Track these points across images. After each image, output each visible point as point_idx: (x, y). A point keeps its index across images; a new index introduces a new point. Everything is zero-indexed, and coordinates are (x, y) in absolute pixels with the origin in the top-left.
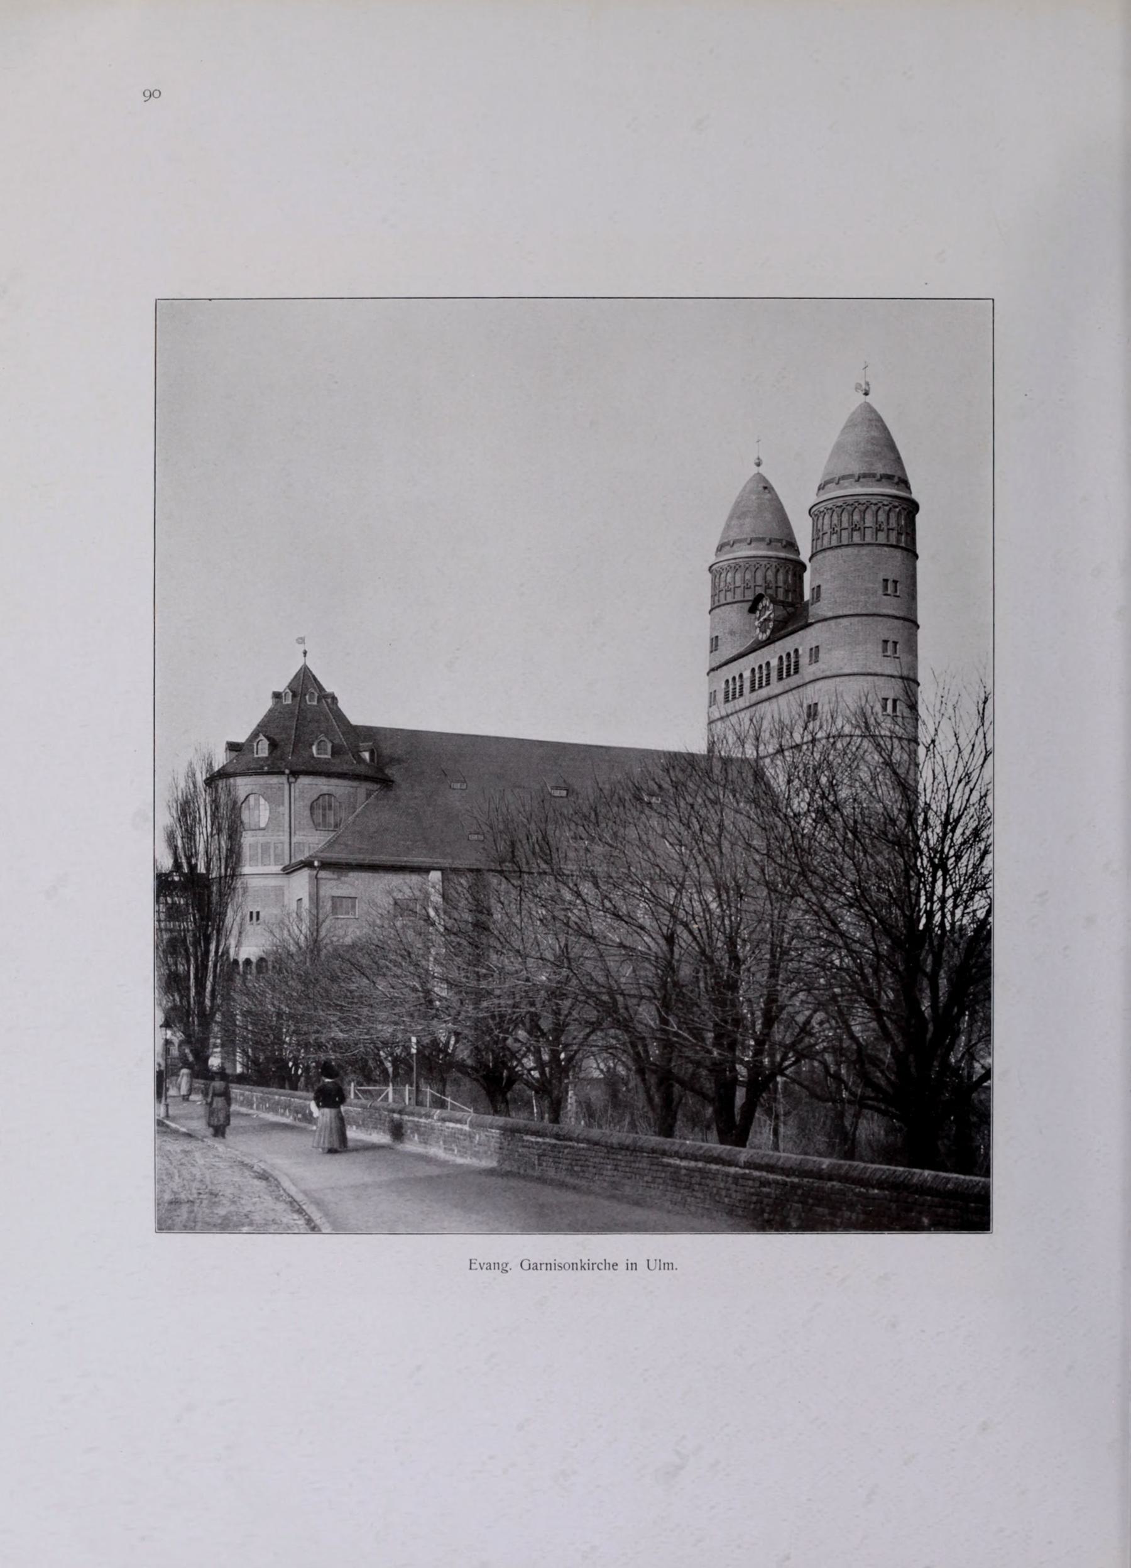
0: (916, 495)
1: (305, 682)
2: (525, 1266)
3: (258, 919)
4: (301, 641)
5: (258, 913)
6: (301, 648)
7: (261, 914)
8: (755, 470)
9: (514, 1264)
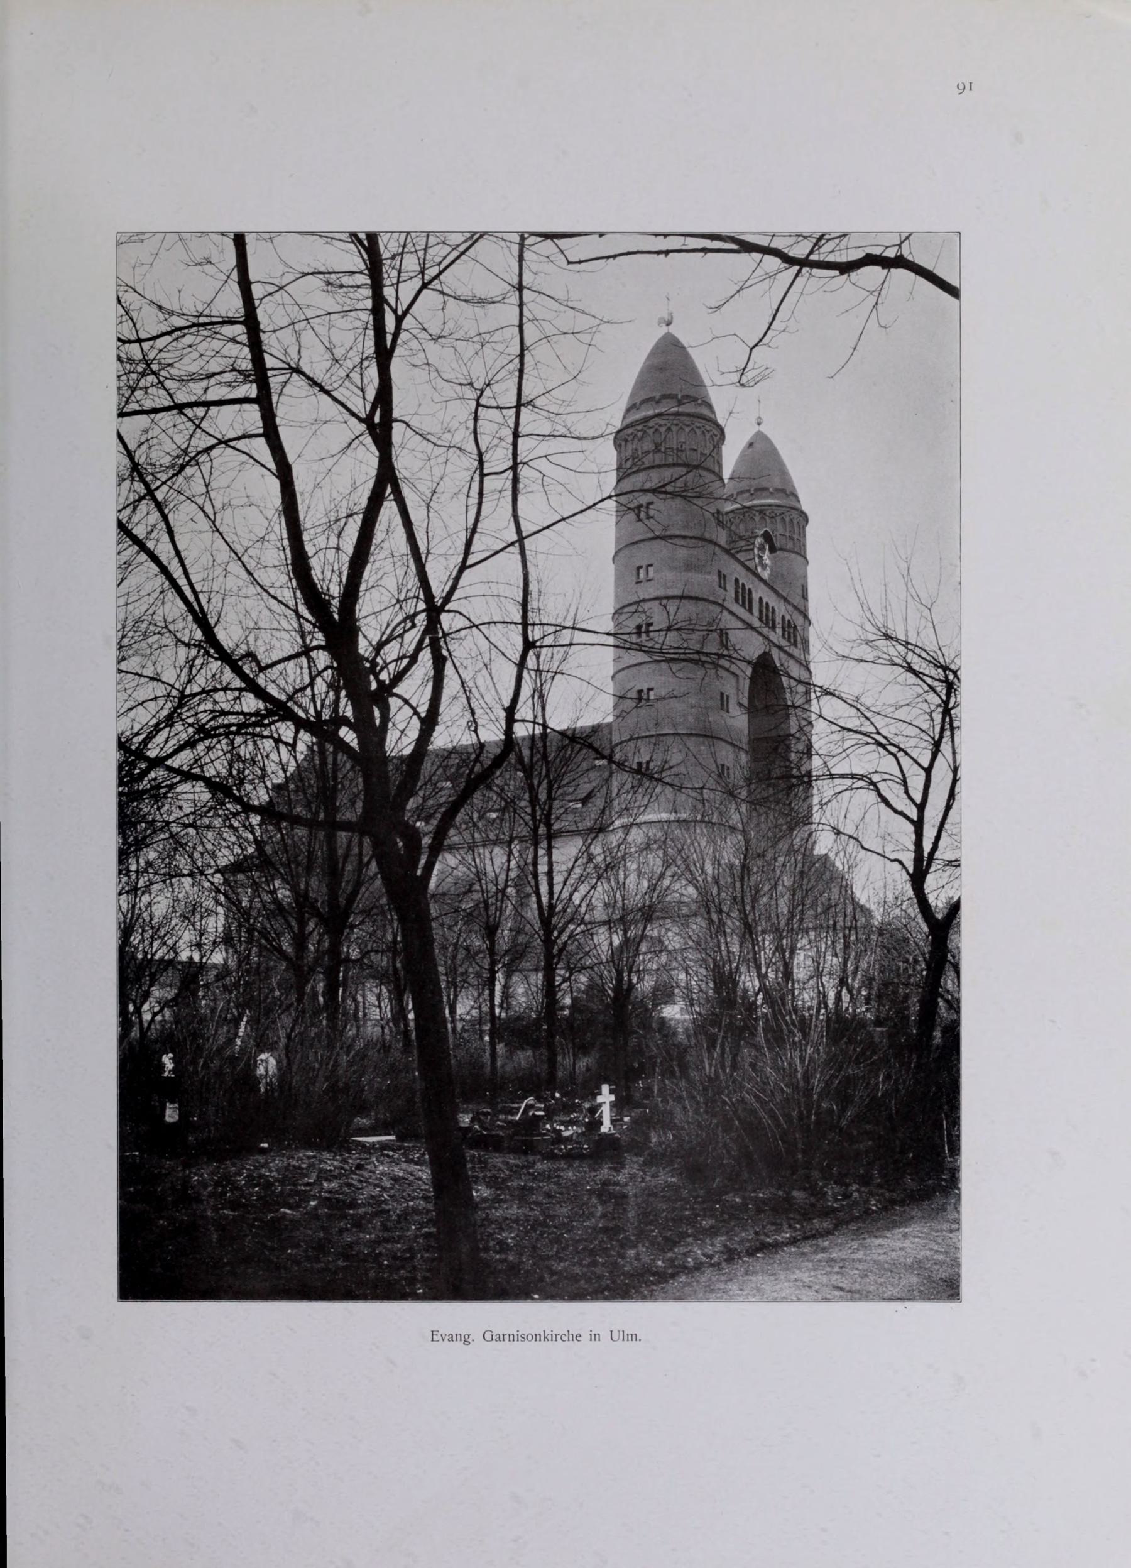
2: (488, 1337)
9: (477, 1336)
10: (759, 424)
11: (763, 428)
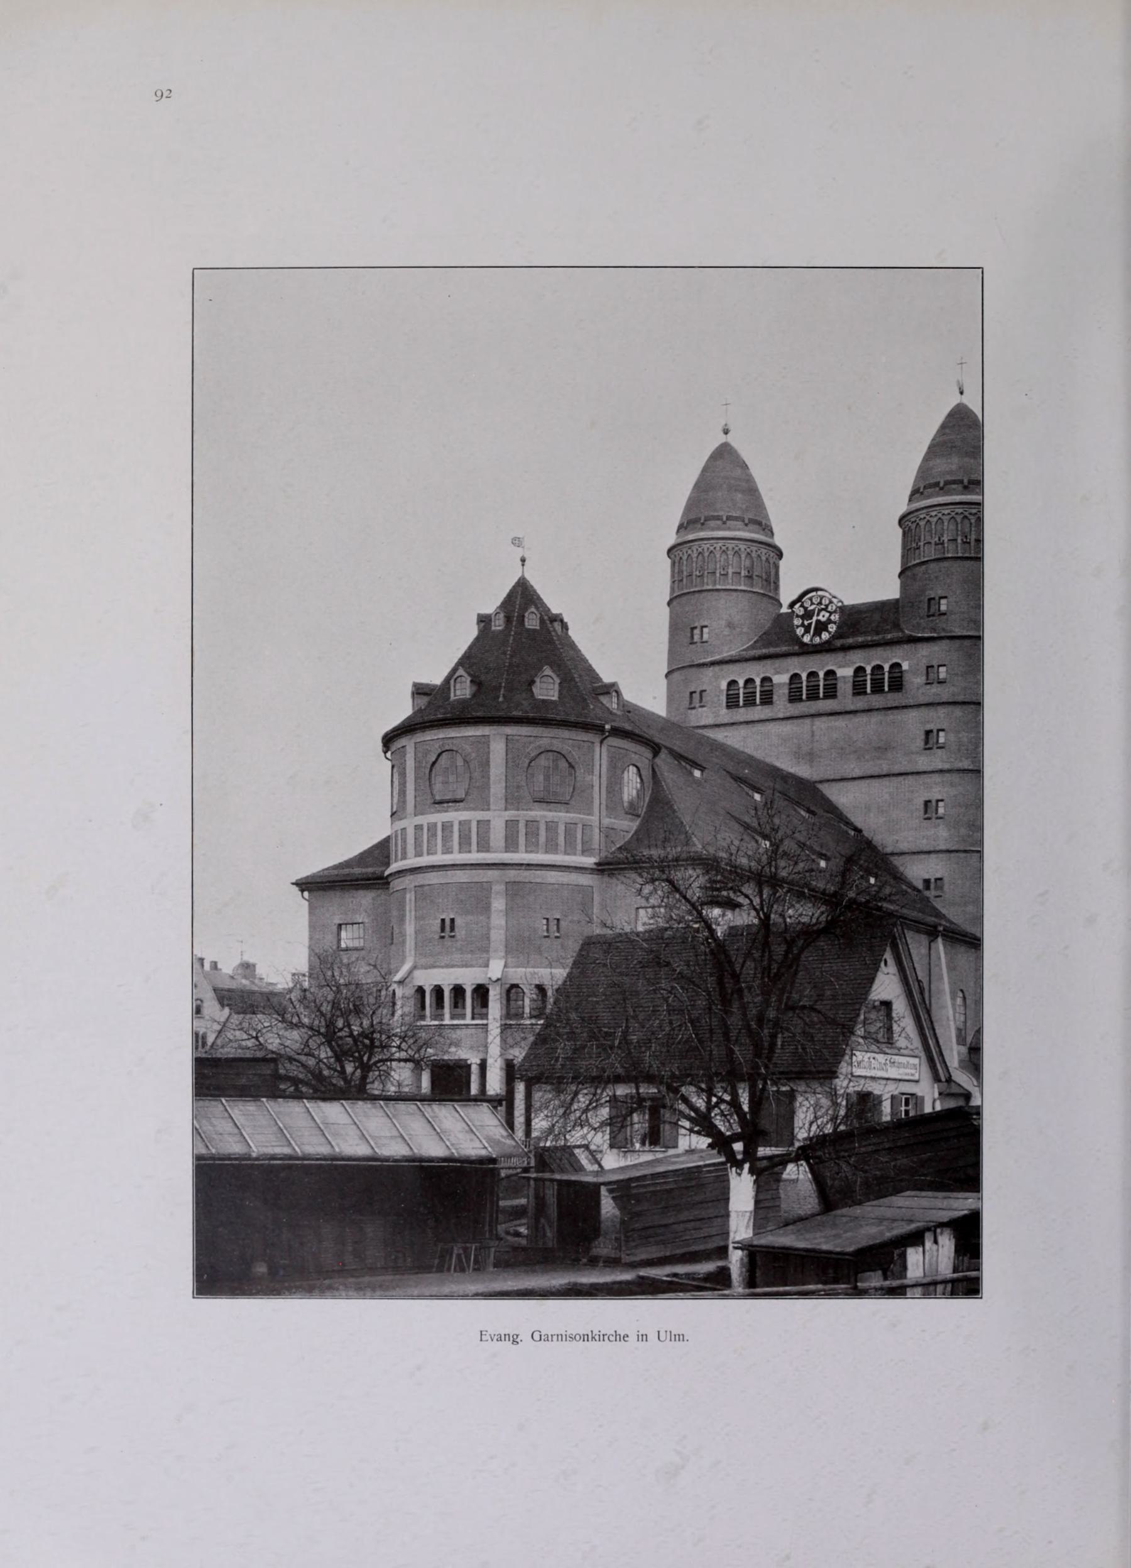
0: (778, 541)
1: (522, 596)
2: (537, 1337)
3: (452, 929)
4: (517, 542)
5: (452, 920)
6: (519, 552)
7: (458, 922)
9: (525, 1336)
10: (726, 432)
11: (730, 439)
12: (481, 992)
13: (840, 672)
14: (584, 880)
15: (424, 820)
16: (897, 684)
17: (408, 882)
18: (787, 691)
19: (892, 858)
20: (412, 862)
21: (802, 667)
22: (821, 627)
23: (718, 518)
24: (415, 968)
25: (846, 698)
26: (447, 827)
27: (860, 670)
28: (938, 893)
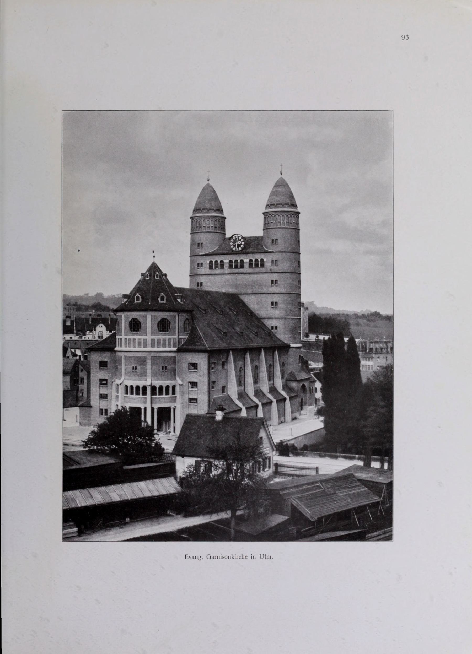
1: (154, 269)
2: (209, 557)
5: (136, 367)
6: (153, 254)
8: (280, 176)
9: (204, 557)
12: (145, 388)
13: (245, 261)
14: (173, 354)
15: (128, 337)
16: (263, 265)
17: (123, 355)
18: (228, 265)
19: (262, 320)
20: (123, 349)
21: (233, 258)
22: (239, 246)
23: (207, 209)
24: (124, 379)
25: (246, 268)
26: (134, 340)
27: (251, 260)
28: (276, 331)
